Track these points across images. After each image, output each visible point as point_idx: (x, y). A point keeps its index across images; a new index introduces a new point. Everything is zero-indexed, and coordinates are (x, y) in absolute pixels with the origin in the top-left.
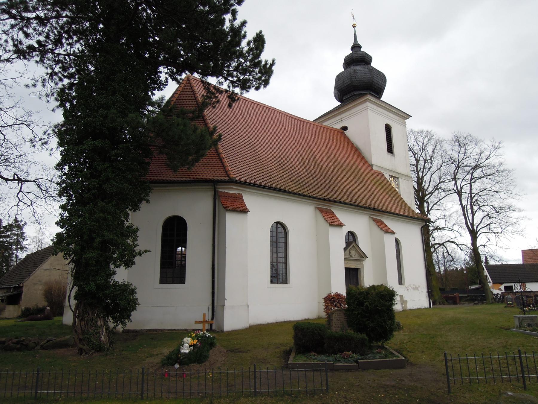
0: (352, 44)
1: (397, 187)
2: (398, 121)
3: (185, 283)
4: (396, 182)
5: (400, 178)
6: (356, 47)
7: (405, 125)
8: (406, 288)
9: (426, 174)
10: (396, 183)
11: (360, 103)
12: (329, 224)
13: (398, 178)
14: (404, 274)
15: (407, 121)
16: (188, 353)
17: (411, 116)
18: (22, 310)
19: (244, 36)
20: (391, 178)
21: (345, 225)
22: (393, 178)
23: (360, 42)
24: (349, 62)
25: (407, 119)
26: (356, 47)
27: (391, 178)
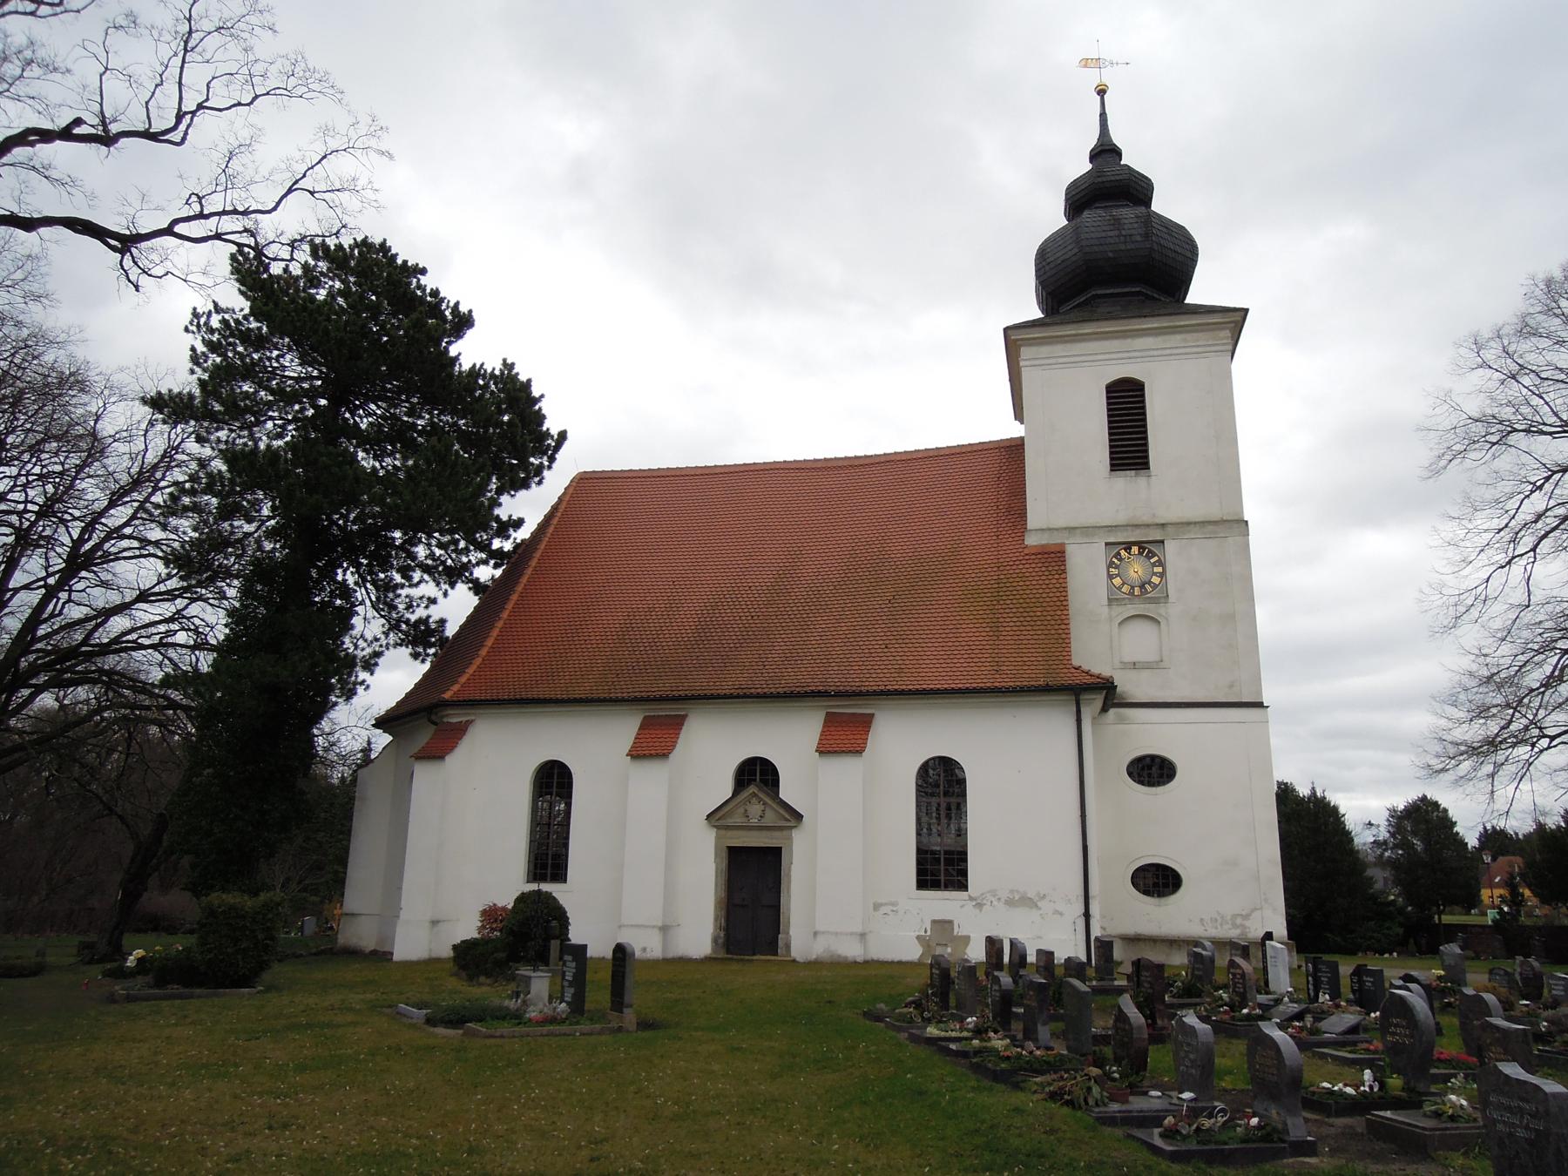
0: (1092, 141)
2: (1188, 350)
4: (1154, 555)
6: (1105, 151)
8: (971, 899)
23: (1117, 138)
24: (1081, 198)
26: (1105, 151)
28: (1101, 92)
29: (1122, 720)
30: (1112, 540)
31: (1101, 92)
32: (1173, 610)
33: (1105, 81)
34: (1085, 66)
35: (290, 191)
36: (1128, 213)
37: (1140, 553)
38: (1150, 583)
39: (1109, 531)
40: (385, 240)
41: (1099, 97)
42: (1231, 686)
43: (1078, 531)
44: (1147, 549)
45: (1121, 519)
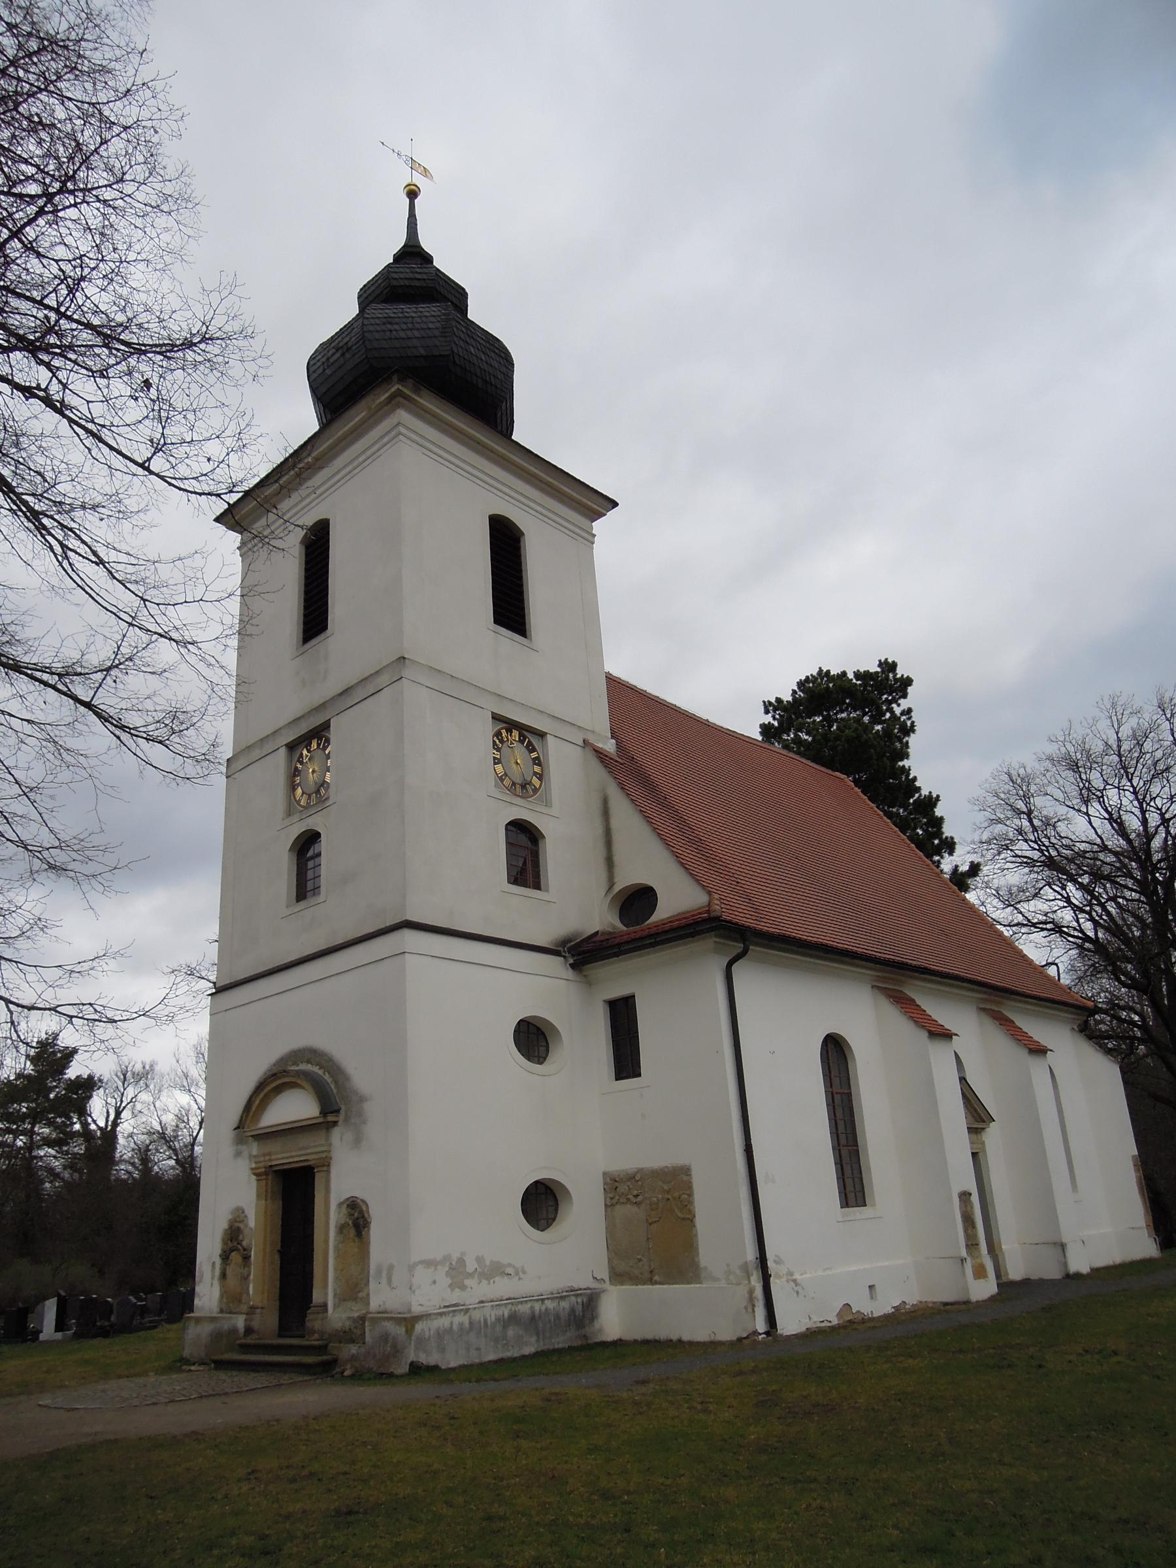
1: (535, 774)
3: (639, 1075)
5: (549, 738)
7: (590, 538)
9: (117, 443)
10: (534, 755)
11: (352, 431)
12: (1027, 1051)
13: (542, 735)
14: (863, 1122)
15: (598, 526)
16: (167, 1182)
17: (615, 504)
18: (56, 1036)
19: (769, 723)
20: (509, 731)
21: (956, 1035)
22: (515, 734)
23: (427, 243)
25: (601, 515)
27: (509, 731)
28: (412, 194)
31: (412, 194)
38: (530, 783)
41: (408, 200)
44: (319, 734)
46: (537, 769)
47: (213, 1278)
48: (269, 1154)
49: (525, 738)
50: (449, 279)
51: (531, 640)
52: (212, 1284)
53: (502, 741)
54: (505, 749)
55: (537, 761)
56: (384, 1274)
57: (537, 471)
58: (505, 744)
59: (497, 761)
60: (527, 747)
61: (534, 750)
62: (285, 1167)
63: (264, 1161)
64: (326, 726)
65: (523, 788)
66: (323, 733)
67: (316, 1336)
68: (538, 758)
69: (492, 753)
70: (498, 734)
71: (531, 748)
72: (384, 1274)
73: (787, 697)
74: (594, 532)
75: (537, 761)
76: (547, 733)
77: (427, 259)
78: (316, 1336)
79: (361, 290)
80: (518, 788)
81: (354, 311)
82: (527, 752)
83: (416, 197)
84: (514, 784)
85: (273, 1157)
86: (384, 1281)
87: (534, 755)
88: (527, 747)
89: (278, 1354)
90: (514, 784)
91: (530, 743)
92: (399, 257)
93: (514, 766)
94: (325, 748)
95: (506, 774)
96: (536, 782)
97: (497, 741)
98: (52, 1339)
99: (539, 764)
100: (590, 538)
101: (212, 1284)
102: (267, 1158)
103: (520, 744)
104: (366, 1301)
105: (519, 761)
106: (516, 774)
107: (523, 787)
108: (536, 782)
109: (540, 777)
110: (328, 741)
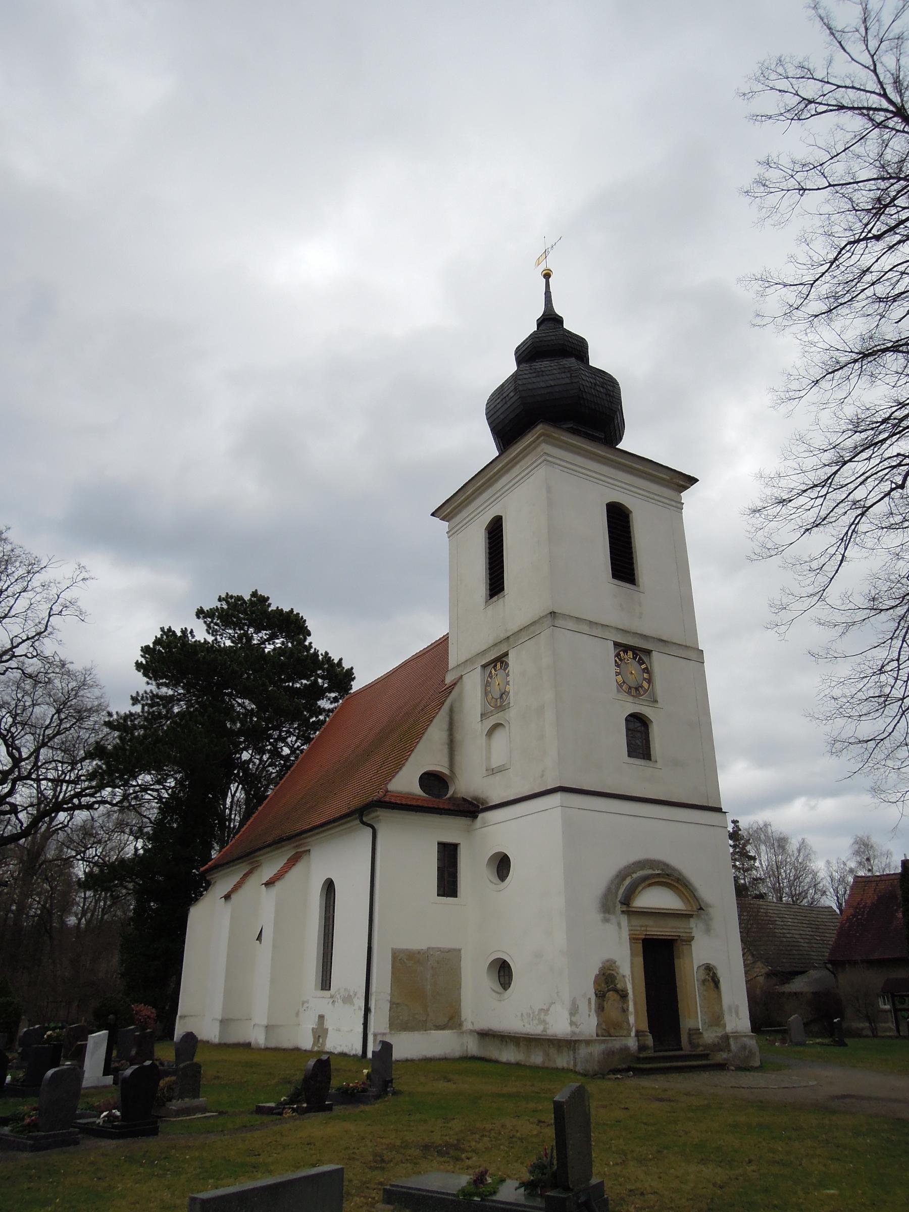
0: (540, 312)
1: (645, 679)
7: (679, 506)
8: (332, 997)
10: (643, 666)
13: (648, 652)
15: (685, 496)
22: (630, 653)
23: (558, 310)
25: (686, 488)
28: (547, 276)
29: (485, 825)
30: (484, 662)
31: (547, 276)
32: (512, 714)
33: (549, 267)
34: (539, 264)
35: (50, 616)
36: (572, 362)
37: (501, 667)
38: (642, 687)
39: (482, 655)
40: (256, 590)
41: (545, 280)
42: (542, 776)
43: (468, 662)
44: (501, 661)
45: (491, 642)
46: (646, 676)
47: (590, 1011)
48: (647, 926)
49: (637, 655)
50: (524, 342)
51: (639, 586)
52: (589, 1015)
53: (620, 660)
54: (623, 665)
55: (645, 670)
56: (733, 1011)
57: (627, 462)
58: (623, 662)
59: (617, 674)
60: (638, 662)
61: (644, 663)
62: (655, 937)
63: (640, 930)
64: (506, 654)
65: (635, 691)
66: (503, 659)
67: (701, 1048)
68: (647, 668)
69: (613, 669)
70: (618, 655)
71: (641, 662)
72: (733, 1011)
73: (352, 683)
74: (682, 501)
75: (645, 670)
76: (652, 651)
77: (559, 321)
78: (701, 1048)
79: (517, 349)
80: (633, 691)
81: (511, 367)
82: (638, 665)
83: (550, 277)
84: (630, 688)
85: (648, 929)
86: (734, 1015)
87: (643, 666)
88: (638, 662)
89: (677, 1061)
90: (630, 688)
91: (640, 659)
92: (541, 322)
93: (629, 675)
94: (505, 670)
95: (624, 682)
96: (645, 685)
97: (618, 660)
98: (100, 1084)
99: (648, 672)
100: (679, 505)
101: (589, 1015)
102: (643, 929)
103: (634, 661)
104: (724, 1026)
105: (633, 672)
106: (632, 681)
107: (637, 689)
108: (645, 685)
109: (650, 681)
110: (507, 665)
